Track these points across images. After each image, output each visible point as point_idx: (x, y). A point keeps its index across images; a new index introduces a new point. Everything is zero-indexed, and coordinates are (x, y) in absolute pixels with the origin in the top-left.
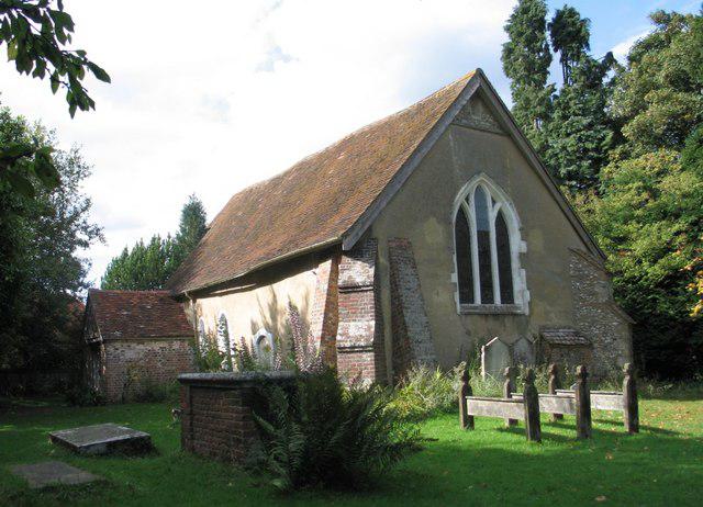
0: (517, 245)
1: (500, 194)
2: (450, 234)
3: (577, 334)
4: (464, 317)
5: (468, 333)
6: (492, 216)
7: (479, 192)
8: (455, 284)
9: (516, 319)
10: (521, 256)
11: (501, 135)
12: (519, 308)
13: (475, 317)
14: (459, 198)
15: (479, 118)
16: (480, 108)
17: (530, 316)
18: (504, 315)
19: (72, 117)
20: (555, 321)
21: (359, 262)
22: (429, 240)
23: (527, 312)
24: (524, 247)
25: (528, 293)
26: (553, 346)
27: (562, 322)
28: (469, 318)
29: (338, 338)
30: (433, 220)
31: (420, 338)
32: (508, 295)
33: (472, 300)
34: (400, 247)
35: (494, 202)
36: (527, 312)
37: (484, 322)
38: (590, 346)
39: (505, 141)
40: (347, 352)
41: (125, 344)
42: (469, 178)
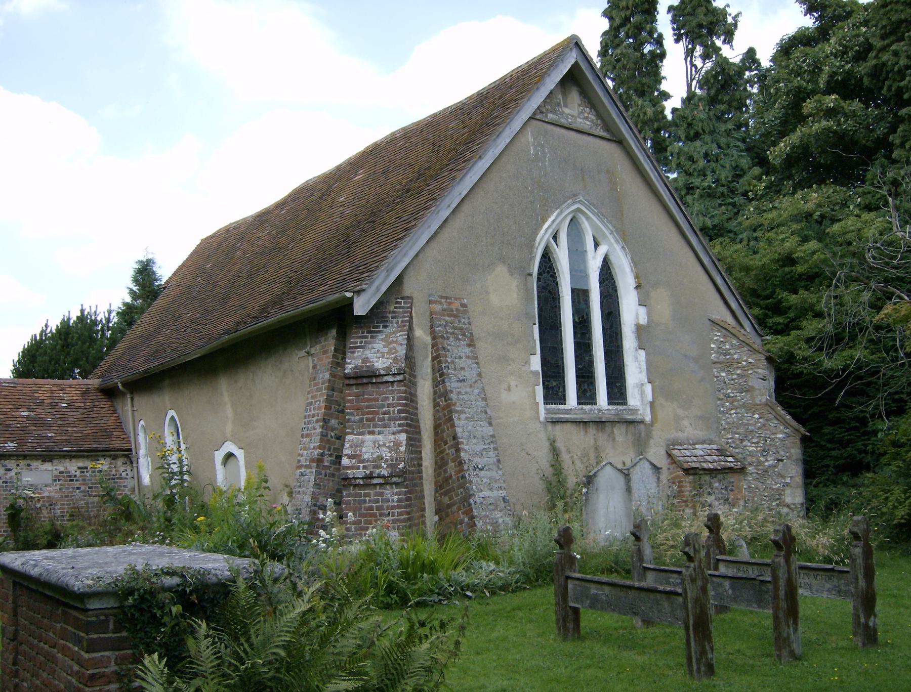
0: (631, 312)
3: (721, 452)
4: (550, 427)
9: (632, 426)
13: (568, 427)
14: (543, 237)
15: (575, 113)
25: (648, 388)
27: (700, 434)
28: (558, 427)
30: (501, 270)
33: (563, 400)
38: (742, 470)
41: (22, 463)
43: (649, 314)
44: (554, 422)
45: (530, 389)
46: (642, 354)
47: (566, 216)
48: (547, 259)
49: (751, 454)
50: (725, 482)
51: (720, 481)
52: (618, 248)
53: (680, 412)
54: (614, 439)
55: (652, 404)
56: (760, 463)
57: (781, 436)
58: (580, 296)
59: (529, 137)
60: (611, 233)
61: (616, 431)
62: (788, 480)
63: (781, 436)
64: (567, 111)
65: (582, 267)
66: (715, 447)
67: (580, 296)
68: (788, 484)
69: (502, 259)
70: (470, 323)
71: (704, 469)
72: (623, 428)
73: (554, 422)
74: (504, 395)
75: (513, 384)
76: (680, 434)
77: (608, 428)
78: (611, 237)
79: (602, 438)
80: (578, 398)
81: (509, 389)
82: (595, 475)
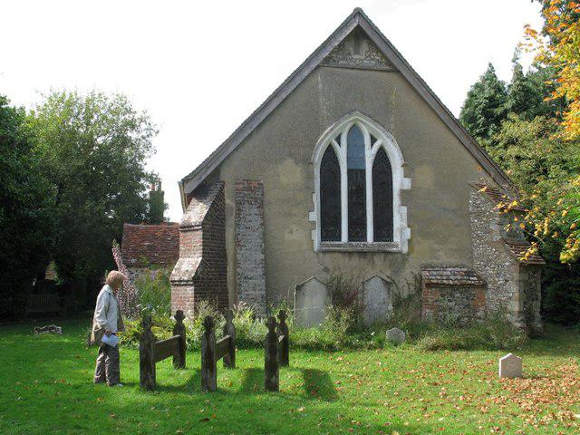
0: (399, 181)
1: (378, 130)
2: (310, 177)
3: (469, 274)
4: (321, 255)
5: (326, 270)
6: (370, 155)
7: (355, 132)
8: (314, 222)
9: (390, 256)
10: (403, 192)
11: (389, 71)
12: (397, 246)
13: (336, 255)
14: (325, 139)
15: (363, 58)
16: (365, 46)
17: (408, 254)
18: (373, 253)
19: (490, 65)
20: (443, 258)
21: (201, 204)
22: (284, 180)
23: (405, 250)
24: (407, 184)
25: (408, 231)
26: (429, 285)
27: (453, 261)
28: (328, 255)
29: (173, 272)
30: (290, 162)
31: (250, 274)
32: (384, 228)
33: (364, 238)
34: (249, 189)
35: (373, 140)
36: (405, 250)
37: (347, 259)
38: (484, 286)
39: (393, 77)
40: (178, 285)
41: (139, 270)
42: (338, 115)
43: (413, 182)
44: (325, 252)
45: (307, 232)
46: (404, 209)
47: (346, 125)
48: (330, 154)
49: (491, 275)
50: (467, 294)
51: (461, 293)
52: (389, 141)
53: (436, 246)
54: (374, 263)
55: (409, 241)
56: (496, 282)
57: (507, 264)
58: (356, 175)
59: (319, 78)
60: (384, 132)
61: (375, 258)
62: (511, 295)
63: (507, 264)
64: (355, 57)
65: (361, 155)
66: (465, 270)
67: (356, 175)
68: (511, 298)
69: (291, 155)
70: (262, 195)
71: (444, 284)
72: (382, 256)
73: (325, 252)
74: (287, 236)
75: (294, 229)
76: (435, 261)
77: (369, 256)
78: (383, 134)
79: (364, 262)
80: (349, 237)
81: (291, 232)
82: (303, 285)
